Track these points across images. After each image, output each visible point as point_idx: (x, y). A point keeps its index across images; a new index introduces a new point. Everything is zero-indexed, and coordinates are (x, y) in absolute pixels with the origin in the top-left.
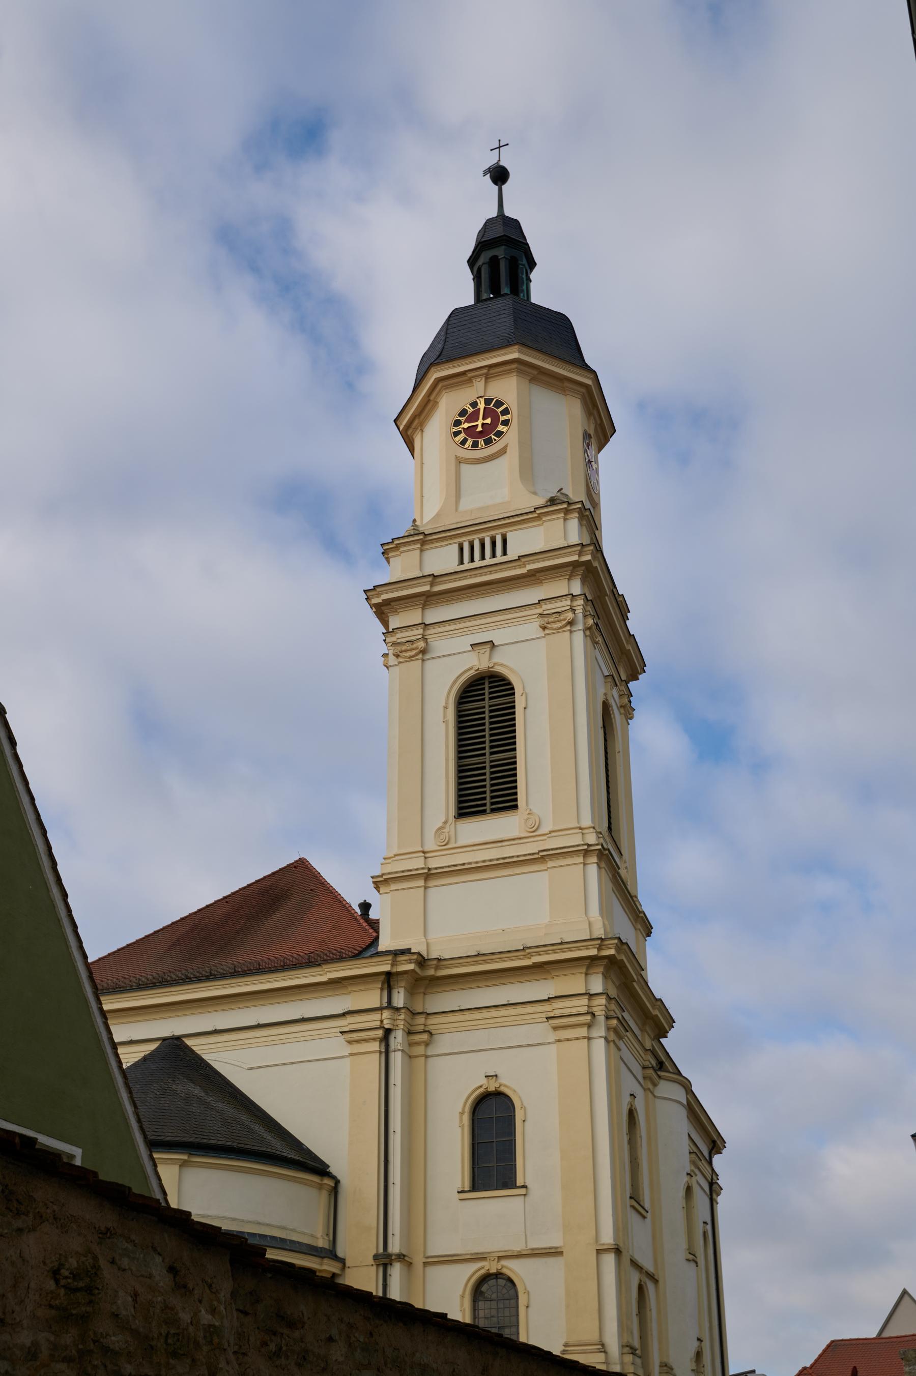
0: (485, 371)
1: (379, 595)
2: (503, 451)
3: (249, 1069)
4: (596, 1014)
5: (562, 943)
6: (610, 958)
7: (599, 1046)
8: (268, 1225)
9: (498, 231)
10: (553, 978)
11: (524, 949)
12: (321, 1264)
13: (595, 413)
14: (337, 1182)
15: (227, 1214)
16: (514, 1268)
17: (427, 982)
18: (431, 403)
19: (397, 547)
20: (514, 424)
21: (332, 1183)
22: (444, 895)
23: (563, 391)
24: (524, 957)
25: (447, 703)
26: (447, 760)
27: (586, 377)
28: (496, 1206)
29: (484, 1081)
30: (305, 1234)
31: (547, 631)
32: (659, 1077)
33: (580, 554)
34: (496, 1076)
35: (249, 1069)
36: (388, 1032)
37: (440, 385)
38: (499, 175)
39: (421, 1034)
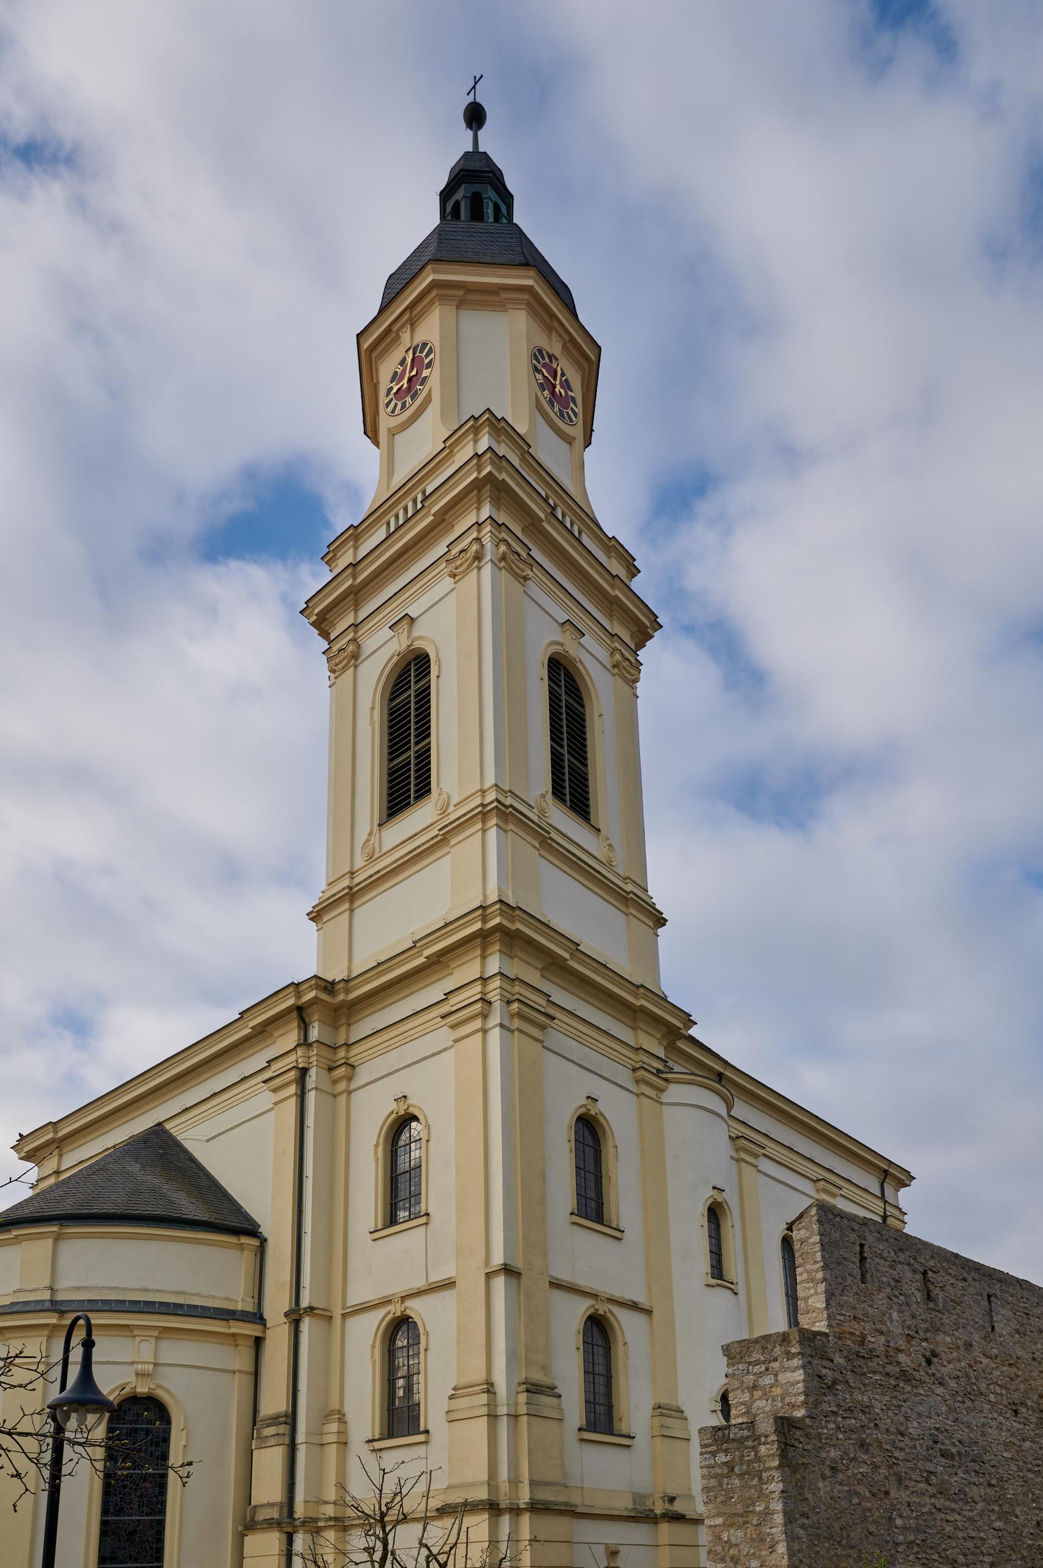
0: (407, 316)
2: (428, 400)
3: (208, 1141)
4: (493, 1000)
5: (447, 925)
6: (499, 928)
7: (495, 1036)
8: (158, 1291)
12: (230, 1328)
13: (555, 324)
14: (264, 1241)
17: (344, 1011)
20: (437, 364)
21: (256, 1242)
22: (368, 911)
23: (502, 306)
25: (373, 704)
26: (373, 765)
27: (525, 277)
28: (407, 1242)
29: (393, 1106)
30: (214, 1297)
31: (457, 578)
32: (667, 1080)
33: (479, 468)
34: (405, 1097)
35: (208, 1141)
36: (304, 1072)
39: (341, 1066)
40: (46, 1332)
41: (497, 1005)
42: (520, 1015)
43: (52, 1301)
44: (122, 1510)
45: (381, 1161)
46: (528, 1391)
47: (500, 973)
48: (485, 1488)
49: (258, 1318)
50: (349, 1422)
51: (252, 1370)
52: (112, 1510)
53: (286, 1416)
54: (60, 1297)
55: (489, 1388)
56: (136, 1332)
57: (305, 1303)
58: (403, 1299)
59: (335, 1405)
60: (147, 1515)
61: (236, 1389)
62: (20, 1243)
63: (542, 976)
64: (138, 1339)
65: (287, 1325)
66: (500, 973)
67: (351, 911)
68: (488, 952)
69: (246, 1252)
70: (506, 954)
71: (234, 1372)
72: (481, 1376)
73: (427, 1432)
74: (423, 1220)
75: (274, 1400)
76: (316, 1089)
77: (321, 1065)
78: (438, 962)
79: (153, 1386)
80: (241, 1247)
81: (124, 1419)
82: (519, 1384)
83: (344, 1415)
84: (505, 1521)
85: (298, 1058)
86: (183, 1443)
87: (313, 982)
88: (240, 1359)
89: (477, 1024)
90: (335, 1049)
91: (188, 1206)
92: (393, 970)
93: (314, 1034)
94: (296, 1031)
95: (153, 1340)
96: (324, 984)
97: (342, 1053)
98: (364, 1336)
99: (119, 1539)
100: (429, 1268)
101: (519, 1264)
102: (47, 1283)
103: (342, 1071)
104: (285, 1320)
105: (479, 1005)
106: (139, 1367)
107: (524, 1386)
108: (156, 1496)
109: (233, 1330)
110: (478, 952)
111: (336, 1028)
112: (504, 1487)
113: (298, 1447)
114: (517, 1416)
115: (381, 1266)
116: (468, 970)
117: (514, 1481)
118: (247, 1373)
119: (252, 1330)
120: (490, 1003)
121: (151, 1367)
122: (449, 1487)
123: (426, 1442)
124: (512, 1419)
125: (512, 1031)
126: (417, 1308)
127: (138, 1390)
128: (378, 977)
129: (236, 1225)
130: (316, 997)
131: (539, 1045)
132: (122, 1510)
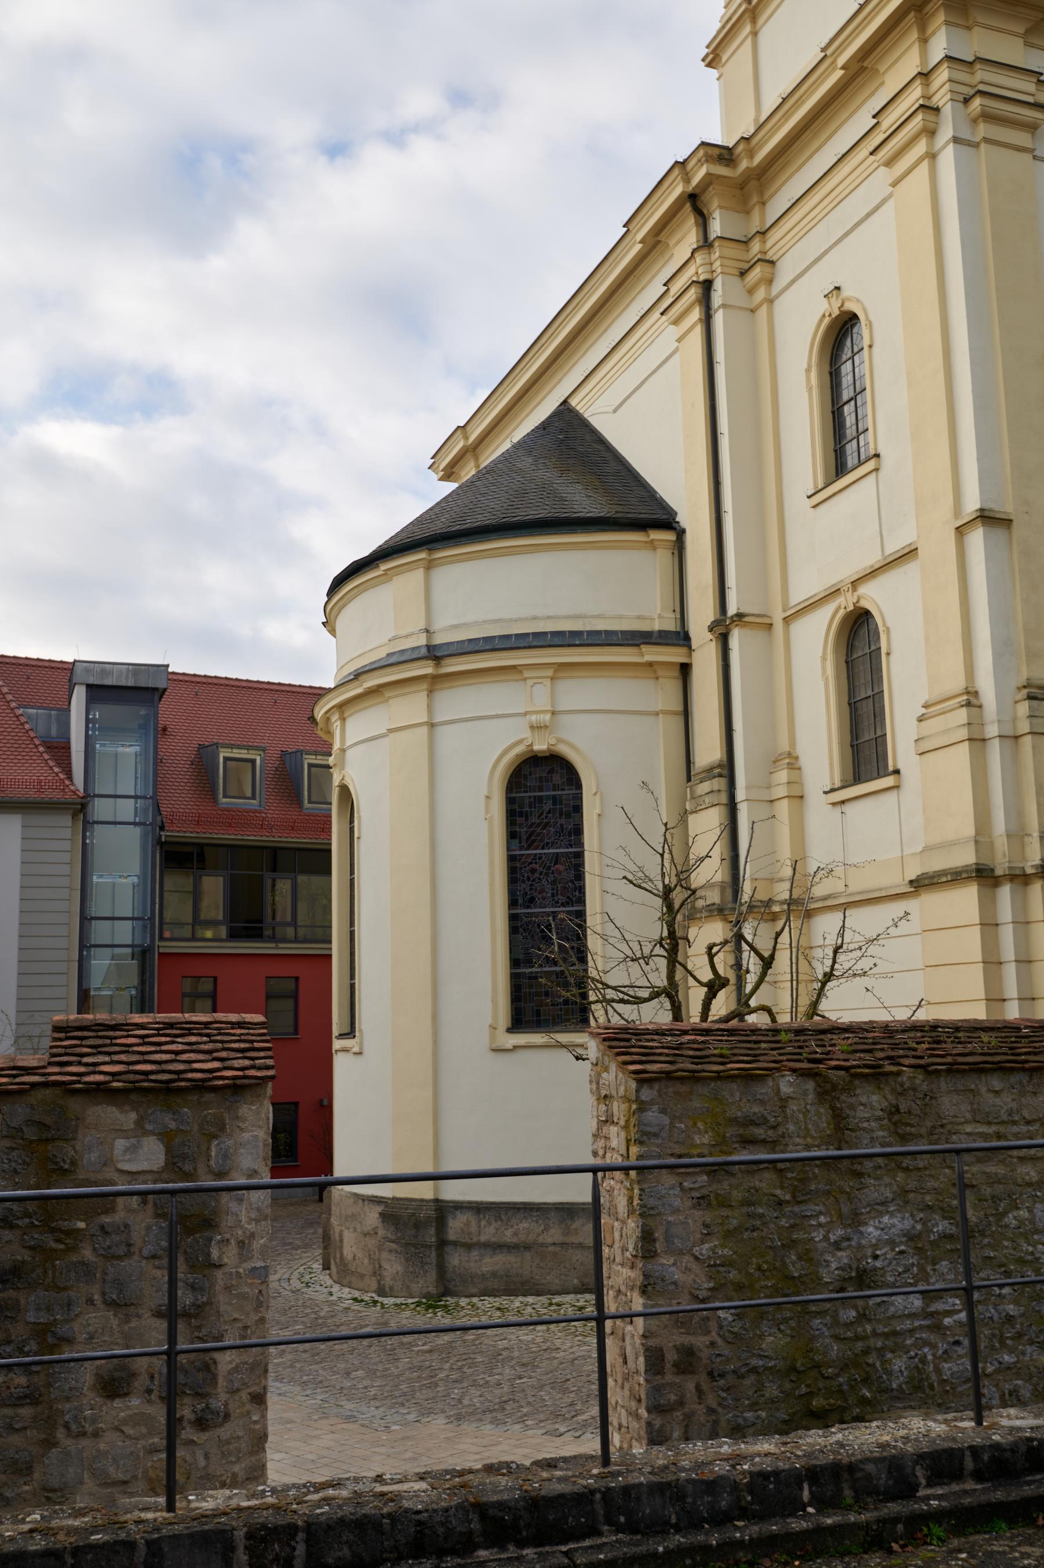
3: (615, 411)
4: (940, 104)
7: (948, 158)
14: (681, 533)
15: (491, 616)
21: (670, 536)
28: (858, 496)
30: (621, 617)
34: (838, 288)
35: (615, 411)
36: (707, 286)
39: (755, 264)
40: (425, 686)
41: (947, 111)
42: (987, 116)
43: (429, 647)
44: (532, 900)
45: (815, 392)
46: (1031, 697)
47: (946, 56)
48: (971, 848)
49: (682, 638)
50: (804, 768)
51: (680, 708)
52: (520, 901)
53: (720, 766)
54: (439, 640)
55: (971, 699)
56: (526, 674)
57: (732, 610)
58: (855, 584)
59: (784, 746)
60: (563, 905)
61: (662, 735)
62: (390, 580)
63: (1027, 44)
64: (530, 682)
65: (714, 643)
66: (948, 58)
67: (755, 34)
68: (930, 30)
69: (659, 551)
70: (956, 25)
71: (657, 714)
72: (958, 683)
73: (897, 772)
74: (871, 465)
75: (708, 750)
76: (724, 306)
77: (726, 270)
78: (862, 70)
79: (553, 741)
80: (652, 545)
81: (525, 786)
82: (1019, 688)
83: (797, 758)
84: (1005, 892)
85: (697, 271)
86: (597, 811)
87: (701, 153)
88: (663, 695)
89: (921, 147)
90: (746, 243)
91: (583, 501)
92: (803, 102)
93: (716, 228)
94: (694, 229)
95: (548, 682)
96: (717, 151)
97: (756, 247)
98: (813, 642)
99: (533, 936)
100: (884, 533)
101: (1007, 507)
102: (422, 625)
103: (756, 273)
104: (710, 636)
105: (919, 117)
106: (534, 718)
107: (1025, 691)
108: (572, 882)
109: (648, 658)
110: (914, 35)
111: (748, 212)
112: (1001, 844)
113: (739, 806)
114: (1017, 737)
115: (827, 541)
116: (902, 66)
117: (1017, 836)
118: (675, 713)
119: (674, 655)
120: (937, 110)
121: (548, 717)
122: (927, 849)
123: (897, 787)
124: (1009, 743)
125: (976, 145)
126: (873, 595)
127: (536, 747)
128: (787, 120)
129: (646, 515)
130: (708, 174)
131: (1028, 157)
132: (532, 900)
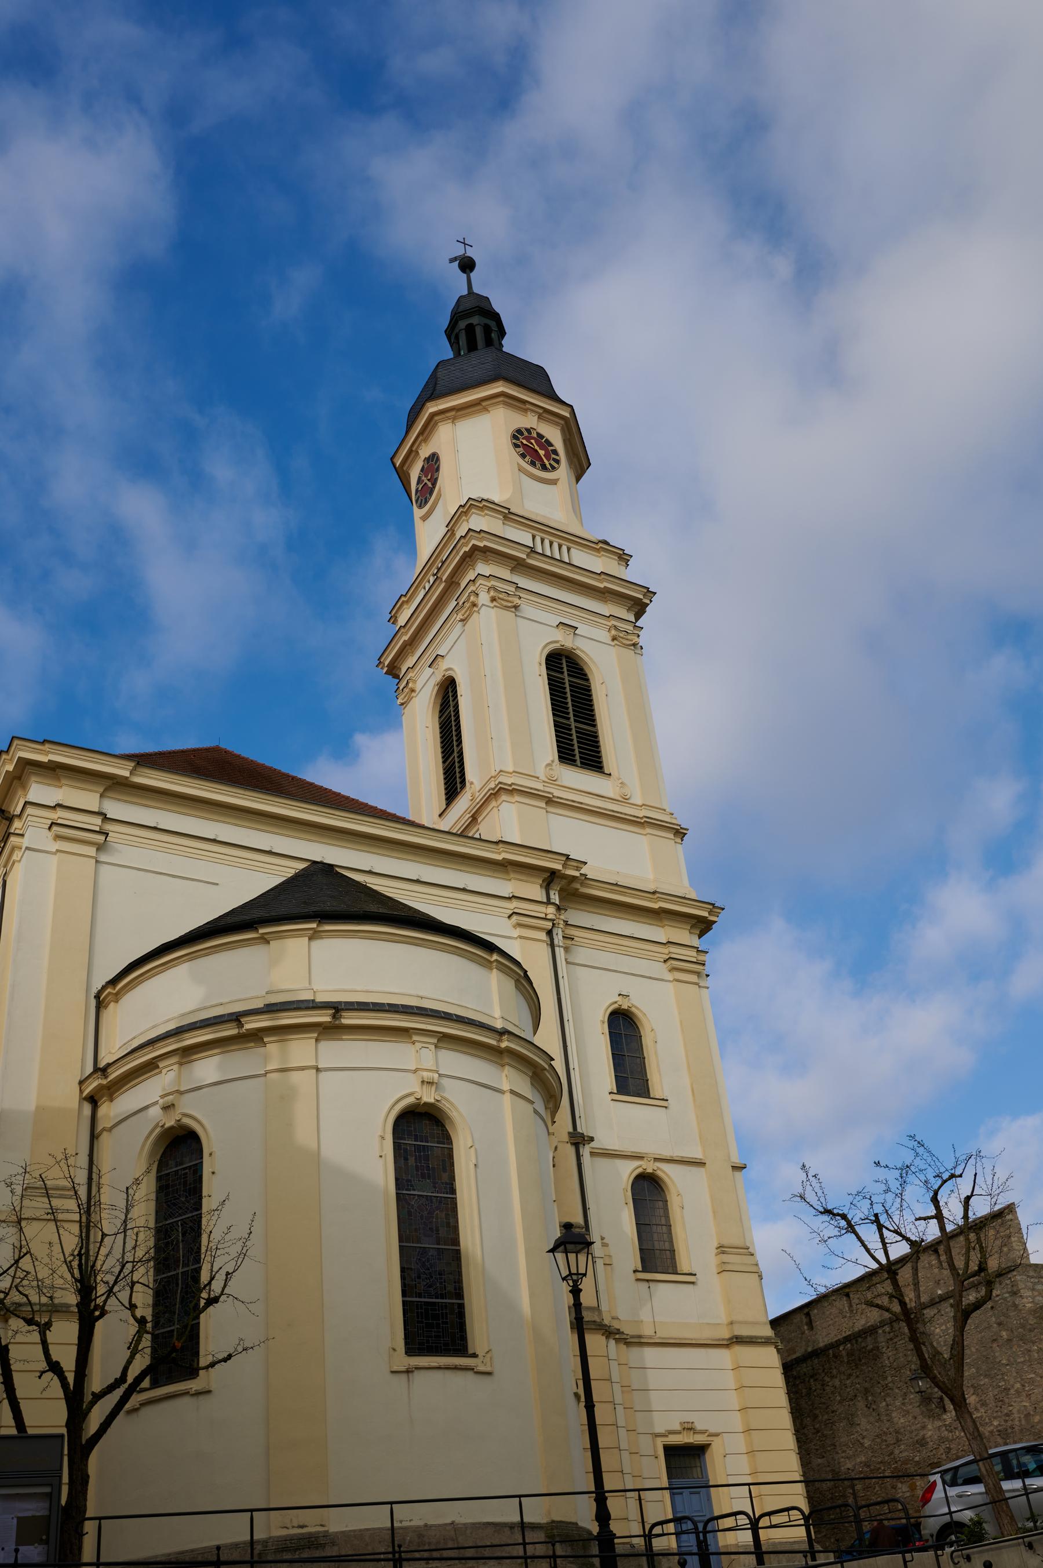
1: (481, 539)
9: (468, 305)
10: (663, 927)
11: (654, 893)
16: (670, 1174)
18: (479, 407)
19: (482, 509)
24: (650, 900)
37: (501, 399)
38: (467, 265)
